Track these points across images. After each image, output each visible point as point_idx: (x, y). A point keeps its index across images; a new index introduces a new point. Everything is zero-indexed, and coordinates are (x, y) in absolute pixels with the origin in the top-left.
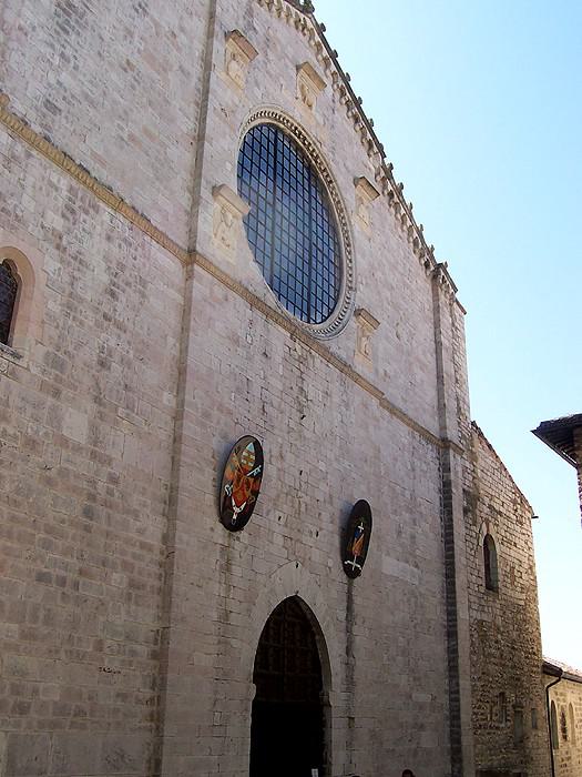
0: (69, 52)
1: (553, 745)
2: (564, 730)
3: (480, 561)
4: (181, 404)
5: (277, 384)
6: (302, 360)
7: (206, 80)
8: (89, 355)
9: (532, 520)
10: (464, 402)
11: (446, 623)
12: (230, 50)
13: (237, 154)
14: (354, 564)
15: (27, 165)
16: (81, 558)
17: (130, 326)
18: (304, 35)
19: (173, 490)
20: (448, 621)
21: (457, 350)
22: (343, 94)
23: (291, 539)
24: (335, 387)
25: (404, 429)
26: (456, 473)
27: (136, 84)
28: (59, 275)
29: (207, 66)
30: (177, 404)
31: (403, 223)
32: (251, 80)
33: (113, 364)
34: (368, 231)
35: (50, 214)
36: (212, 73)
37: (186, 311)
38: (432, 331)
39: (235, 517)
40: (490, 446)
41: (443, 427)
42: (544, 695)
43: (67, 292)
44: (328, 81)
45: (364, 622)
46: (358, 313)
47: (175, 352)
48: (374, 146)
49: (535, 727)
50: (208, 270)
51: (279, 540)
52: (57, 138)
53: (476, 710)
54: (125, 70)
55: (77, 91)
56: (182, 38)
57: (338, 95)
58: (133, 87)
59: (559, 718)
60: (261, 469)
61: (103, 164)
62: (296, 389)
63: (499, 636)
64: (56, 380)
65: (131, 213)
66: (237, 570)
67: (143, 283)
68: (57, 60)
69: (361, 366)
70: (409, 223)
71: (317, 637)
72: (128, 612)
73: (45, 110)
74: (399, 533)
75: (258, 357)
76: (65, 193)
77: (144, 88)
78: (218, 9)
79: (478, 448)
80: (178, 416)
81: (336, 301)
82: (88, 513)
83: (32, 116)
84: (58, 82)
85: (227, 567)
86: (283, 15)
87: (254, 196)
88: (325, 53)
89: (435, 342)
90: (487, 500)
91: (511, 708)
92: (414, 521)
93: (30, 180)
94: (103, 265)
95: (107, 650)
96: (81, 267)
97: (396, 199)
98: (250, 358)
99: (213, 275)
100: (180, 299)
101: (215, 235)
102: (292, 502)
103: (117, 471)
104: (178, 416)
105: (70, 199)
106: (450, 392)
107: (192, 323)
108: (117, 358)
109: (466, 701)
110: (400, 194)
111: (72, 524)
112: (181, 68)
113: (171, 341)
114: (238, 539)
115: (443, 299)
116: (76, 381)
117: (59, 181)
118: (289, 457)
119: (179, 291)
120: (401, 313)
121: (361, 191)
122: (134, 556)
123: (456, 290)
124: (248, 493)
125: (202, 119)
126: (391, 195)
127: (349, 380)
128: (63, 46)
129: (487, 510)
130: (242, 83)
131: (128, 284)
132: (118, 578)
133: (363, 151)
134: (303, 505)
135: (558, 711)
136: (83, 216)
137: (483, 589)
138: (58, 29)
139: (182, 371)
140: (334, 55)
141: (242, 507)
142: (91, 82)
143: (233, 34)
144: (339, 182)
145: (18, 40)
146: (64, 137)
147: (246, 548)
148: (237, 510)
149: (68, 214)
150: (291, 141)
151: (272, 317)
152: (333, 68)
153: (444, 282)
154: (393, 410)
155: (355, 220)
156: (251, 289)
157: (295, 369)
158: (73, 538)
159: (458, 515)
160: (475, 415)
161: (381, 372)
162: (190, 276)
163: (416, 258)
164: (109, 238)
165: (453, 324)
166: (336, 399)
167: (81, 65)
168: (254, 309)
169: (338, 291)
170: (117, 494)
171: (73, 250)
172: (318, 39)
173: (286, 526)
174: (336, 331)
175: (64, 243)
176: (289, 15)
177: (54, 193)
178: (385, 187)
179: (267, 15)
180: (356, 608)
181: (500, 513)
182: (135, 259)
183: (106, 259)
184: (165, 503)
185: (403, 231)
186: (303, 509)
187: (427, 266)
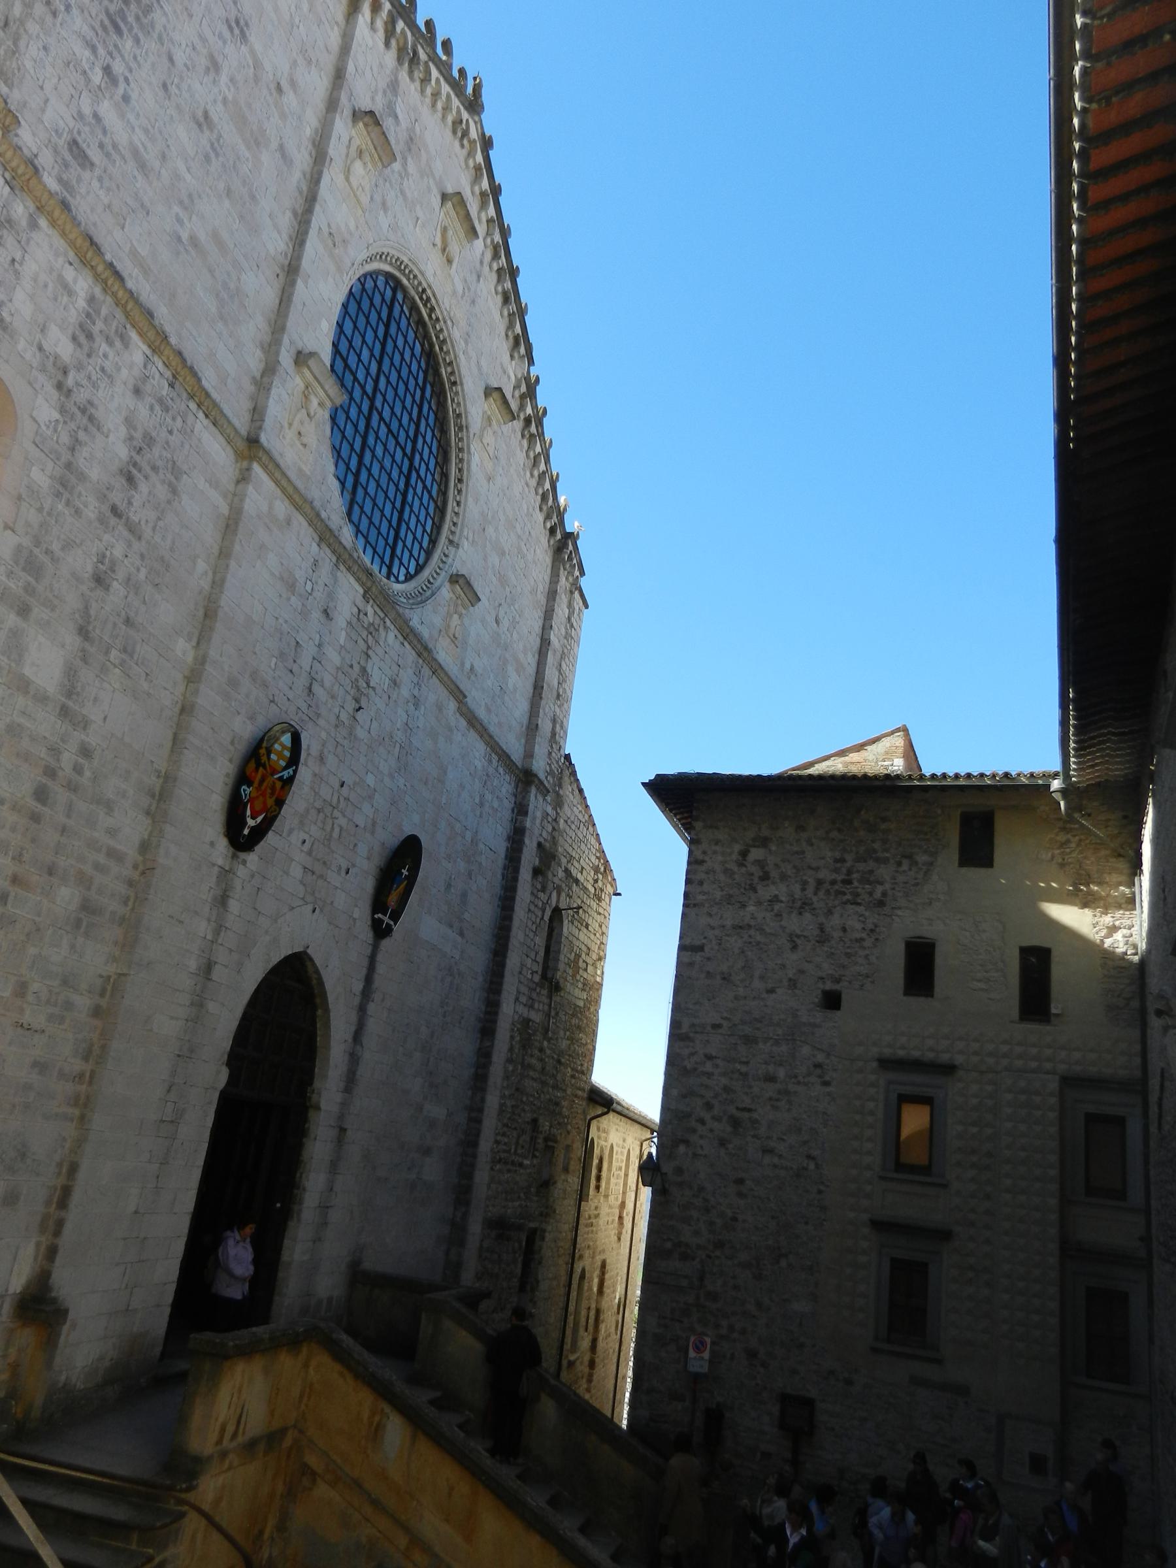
0: (118, 67)
1: (582, 1196)
2: (599, 1178)
3: (540, 941)
4: (202, 660)
5: (333, 656)
6: (372, 630)
7: (314, 180)
8: (82, 562)
9: (613, 897)
10: (562, 727)
11: (482, 1016)
12: (357, 142)
13: (337, 309)
14: (386, 919)
15: (28, 240)
16: (18, 858)
17: (147, 532)
18: (462, 146)
19: (168, 779)
20: (486, 1013)
21: (567, 655)
22: (496, 256)
23: (313, 873)
24: (407, 676)
25: (479, 748)
26: (534, 818)
27: (212, 155)
28: (55, 430)
29: (320, 157)
30: (195, 659)
31: (535, 464)
32: (378, 198)
33: (115, 583)
34: (489, 465)
35: (54, 331)
36: (325, 170)
37: (231, 525)
38: (540, 623)
39: (246, 832)
40: (581, 791)
41: (529, 755)
42: (583, 1128)
43: (63, 459)
44: (481, 229)
45: (383, 1000)
46: (455, 579)
47: (205, 584)
48: (521, 344)
49: (566, 1170)
50: (271, 475)
51: (296, 872)
52: (82, 207)
53: (499, 1138)
54: (200, 125)
55: (122, 138)
56: (290, 99)
57: (489, 255)
58: (207, 159)
59: (595, 1162)
60: (295, 772)
61: (146, 271)
62: (357, 668)
63: (545, 1043)
64: (26, 589)
65: (175, 361)
66: (234, 905)
67: (176, 471)
68: (97, 77)
69: (444, 654)
70: (542, 467)
71: (319, 1012)
72: (72, 947)
73: (69, 157)
74: (449, 886)
75: (316, 615)
76: (81, 303)
77: (223, 165)
78: (351, 68)
79: (567, 790)
80: (194, 677)
81: (429, 554)
82: (41, 794)
83: (46, 160)
84: (96, 116)
85: (222, 900)
86: (439, 105)
87: (349, 378)
88: (485, 184)
89: (542, 639)
90: (564, 861)
91: (540, 1141)
92: (470, 875)
93: (30, 268)
94: (123, 431)
95: (30, 998)
96: (90, 426)
97: (533, 429)
98: (304, 614)
99: (277, 483)
100: (225, 509)
101: (290, 425)
102: (324, 823)
103: (93, 740)
104: (194, 677)
105: (88, 315)
106: (547, 710)
107: (237, 547)
108: (121, 575)
109: (490, 1124)
110: (540, 424)
111: (14, 808)
112: (281, 148)
113: (202, 566)
114: (244, 862)
115: (564, 583)
116: (56, 597)
117: (75, 281)
118: (331, 760)
119: (225, 497)
120: (508, 589)
121: (492, 407)
122: (97, 866)
123: (582, 573)
124: (270, 802)
125: (299, 239)
126: (528, 421)
127: (426, 671)
128: (110, 54)
129: (561, 874)
130: (365, 199)
131: (155, 468)
132: (67, 896)
133: (504, 347)
134: (337, 830)
135: (597, 1152)
136: (104, 347)
137: (537, 978)
138: (107, 22)
139: (209, 613)
140: (496, 191)
141: (259, 819)
142: (146, 131)
143: (368, 118)
144: (465, 387)
145: (42, 22)
146: (92, 210)
147: (253, 876)
148: (251, 822)
149: (82, 339)
150: (414, 308)
151: (344, 562)
152: (491, 211)
153: (570, 558)
154: (473, 721)
155: (475, 446)
156: (324, 515)
157: (361, 642)
158: (13, 829)
159: (525, 874)
160: (572, 746)
161: (468, 666)
162: (243, 478)
163: (540, 517)
164: (137, 391)
165: (569, 619)
166: (405, 692)
167: (134, 96)
168: (323, 545)
169: (433, 542)
170: (88, 774)
171: (81, 396)
172: (479, 158)
173: (310, 853)
174: (421, 598)
175: (70, 382)
176: (447, 108)
177: (65, 299)
178: (522, 407)
179: (417, 96)
180: (378, 981)
181: (577, 881)
182: (171, 432)
183: (129, 422)
184: (153, 796)
185: (532, 475)
186: (335, 834)
187: (552, 531)
